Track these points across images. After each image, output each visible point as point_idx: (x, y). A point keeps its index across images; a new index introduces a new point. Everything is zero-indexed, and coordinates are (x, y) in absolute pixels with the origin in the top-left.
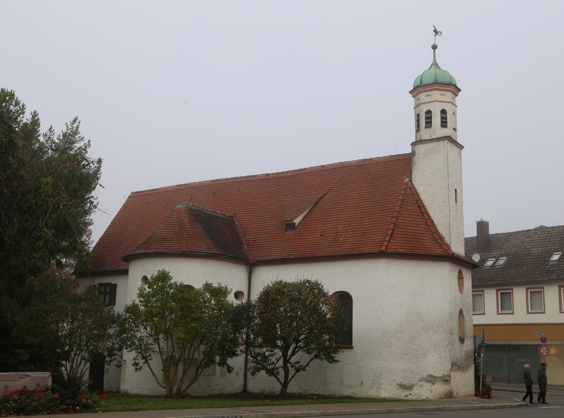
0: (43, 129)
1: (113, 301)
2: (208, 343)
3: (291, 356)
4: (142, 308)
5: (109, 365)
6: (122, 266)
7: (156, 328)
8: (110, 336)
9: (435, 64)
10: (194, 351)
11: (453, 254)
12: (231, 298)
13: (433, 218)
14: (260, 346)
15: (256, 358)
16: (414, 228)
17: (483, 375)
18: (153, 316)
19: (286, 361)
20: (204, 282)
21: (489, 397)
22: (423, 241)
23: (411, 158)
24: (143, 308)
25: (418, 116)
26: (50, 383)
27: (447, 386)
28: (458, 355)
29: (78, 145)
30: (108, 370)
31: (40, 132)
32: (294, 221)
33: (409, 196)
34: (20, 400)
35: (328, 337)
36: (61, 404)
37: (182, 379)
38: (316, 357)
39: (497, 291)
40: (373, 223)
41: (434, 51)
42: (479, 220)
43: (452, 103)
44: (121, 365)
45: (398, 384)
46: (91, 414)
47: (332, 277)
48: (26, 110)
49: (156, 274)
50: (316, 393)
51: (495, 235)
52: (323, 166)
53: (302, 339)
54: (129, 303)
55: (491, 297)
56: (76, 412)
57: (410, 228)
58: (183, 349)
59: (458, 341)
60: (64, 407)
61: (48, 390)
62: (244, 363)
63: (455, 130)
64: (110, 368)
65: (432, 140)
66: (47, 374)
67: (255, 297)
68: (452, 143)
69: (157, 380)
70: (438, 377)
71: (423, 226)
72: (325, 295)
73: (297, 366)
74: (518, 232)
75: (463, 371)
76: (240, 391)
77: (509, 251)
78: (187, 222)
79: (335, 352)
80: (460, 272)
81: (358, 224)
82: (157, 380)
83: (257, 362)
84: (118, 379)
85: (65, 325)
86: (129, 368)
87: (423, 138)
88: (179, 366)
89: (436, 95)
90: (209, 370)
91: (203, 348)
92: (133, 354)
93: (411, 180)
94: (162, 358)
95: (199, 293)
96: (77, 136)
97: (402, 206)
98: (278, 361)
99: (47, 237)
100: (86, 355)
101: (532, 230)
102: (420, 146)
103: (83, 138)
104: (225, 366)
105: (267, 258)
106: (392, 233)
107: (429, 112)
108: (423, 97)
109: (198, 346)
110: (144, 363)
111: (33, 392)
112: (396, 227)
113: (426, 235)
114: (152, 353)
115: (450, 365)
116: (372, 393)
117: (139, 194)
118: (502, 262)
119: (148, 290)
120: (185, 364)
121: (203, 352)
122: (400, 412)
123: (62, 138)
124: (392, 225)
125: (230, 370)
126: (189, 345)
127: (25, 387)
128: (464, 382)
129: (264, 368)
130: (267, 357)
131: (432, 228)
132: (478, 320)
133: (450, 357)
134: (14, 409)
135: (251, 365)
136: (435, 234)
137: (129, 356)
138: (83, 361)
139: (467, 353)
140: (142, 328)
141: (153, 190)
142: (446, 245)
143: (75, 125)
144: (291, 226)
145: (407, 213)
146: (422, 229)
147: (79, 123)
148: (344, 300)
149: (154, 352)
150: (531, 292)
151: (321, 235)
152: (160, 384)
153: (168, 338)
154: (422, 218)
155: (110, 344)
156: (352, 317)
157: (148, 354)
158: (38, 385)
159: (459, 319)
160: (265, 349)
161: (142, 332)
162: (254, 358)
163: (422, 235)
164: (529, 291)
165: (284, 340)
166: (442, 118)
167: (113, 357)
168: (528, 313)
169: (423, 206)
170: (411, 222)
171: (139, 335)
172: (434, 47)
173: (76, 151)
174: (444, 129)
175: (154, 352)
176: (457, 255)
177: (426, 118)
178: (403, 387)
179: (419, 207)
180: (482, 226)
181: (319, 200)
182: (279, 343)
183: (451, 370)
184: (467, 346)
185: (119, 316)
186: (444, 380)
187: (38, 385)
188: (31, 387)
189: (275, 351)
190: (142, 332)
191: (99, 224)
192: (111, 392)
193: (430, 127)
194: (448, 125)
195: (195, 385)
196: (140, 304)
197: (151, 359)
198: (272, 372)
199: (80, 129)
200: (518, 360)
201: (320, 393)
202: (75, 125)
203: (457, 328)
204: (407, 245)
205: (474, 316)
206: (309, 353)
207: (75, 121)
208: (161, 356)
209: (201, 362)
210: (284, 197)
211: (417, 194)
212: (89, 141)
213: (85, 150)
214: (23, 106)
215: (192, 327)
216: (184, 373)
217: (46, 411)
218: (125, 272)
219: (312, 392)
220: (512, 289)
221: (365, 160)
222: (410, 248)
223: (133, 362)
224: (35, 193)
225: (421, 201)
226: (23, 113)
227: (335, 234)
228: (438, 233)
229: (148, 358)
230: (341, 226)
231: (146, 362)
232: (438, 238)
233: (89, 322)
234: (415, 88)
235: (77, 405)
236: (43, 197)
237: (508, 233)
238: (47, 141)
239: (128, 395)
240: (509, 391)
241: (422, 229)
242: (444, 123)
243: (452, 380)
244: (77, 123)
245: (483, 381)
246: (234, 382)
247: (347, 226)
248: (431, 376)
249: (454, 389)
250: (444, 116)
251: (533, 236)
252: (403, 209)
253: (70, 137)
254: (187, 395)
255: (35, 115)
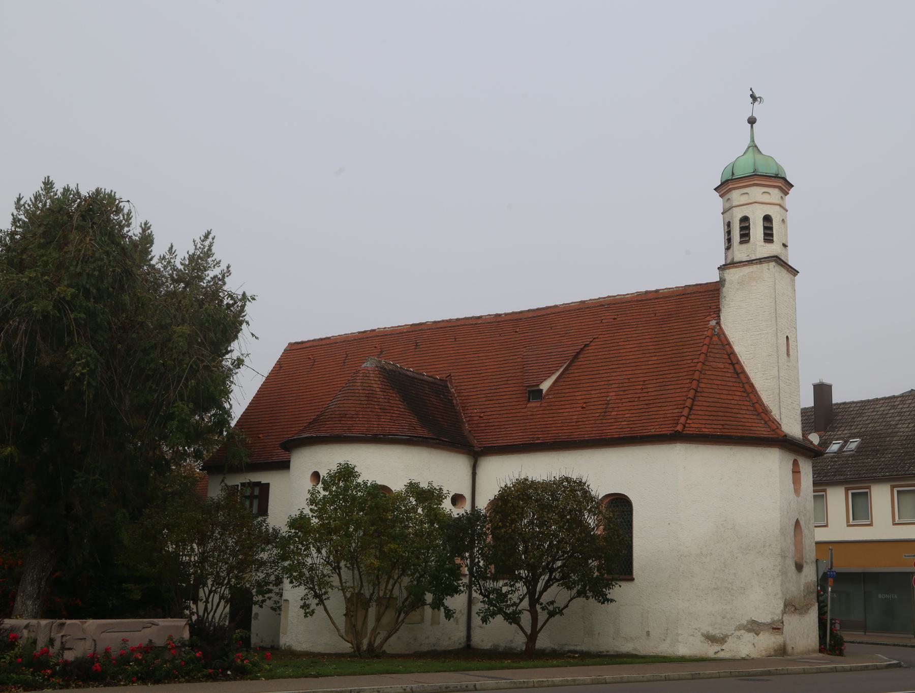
0: (158, 250)
1: (264, 510)
2: (413, 574)
3: (541, 593)
4: (315, 521)
5: (261, 607)
6: (281, 455)
7: (336, 552)
8: (262, 563)
9: (753, 146)
10: (393, 586)
11: (786, 436)
12: (447, 505)
13: (753, 381)
14: (495, 578)
15: (488, 597)
16: (725, 397)
17: (831, 620)
18: (330, 533)
19: (534, 601)
20: (406, 482)
21: (841, 654)
22: (739, 416)
23: (718, 290)
24: (317, 521)
25: (729, 224)
26: (186, 635)
27: (778, 637)
28: (794, 589)
29: (211, 274)
30: (257, 614)
31: (153, 254)
32: (541, 387)
33: (717, 347)
34: (146, 662)
35: (596, 563)
36: (205, 667)
37: (375, 629)
38: (580, 594)
39: (847, 490)
40: (662, 388)
41: (752, 127)
42: (817, 381)
43: (780, 205)
44: (280, 608)
45: (703, 635)
46: (249, 681)
47: (602, 472)
48: (133, 220)
49: (334, 468)
50: (578, 648)
51: (841, 404)
52: (583, 302)
53: (559, 567)
54: (295, 513)
55: (837, 498)
56: (227, 678)
57: (718, 396)
58: (376, 584)
59: (793, 568)
60: (210, 671)
61: (184, 645)
62: (466, 604)
63: (785, 246)
64: (260, 614)
65: (750, 262)
66: (182, 622)
67: (482, 504)
68: (782, 266)
69: (338, 630)
70: (764, 624)
71: (739, 394)
72: (592, 499)
73: (551, 608)
74: (877, 399)
75: (800, 614)
76: (460, 646)
77: (863, 430)
78: (378, 390)
79: (609, 586)
80: (795, 463)
81: (639, 391)
82: (338, 630)
83: (490, 603)
84: (276, 629)
85: (195, 546)
86: (293, 613)
87: (736, 260)
88: (370, 610)
89: (756, 193)
90: (414, 615)
91: (406, 580)
92: (302, 591)
93: (718, 323)
94: (345, 597)
95: (399, 497)
96: (210, 260)
97: (707, 363)
98: (521, 600)
99: (183, 416)
100: (227, 592)
101: (898, 397)
102: (732, 271)
103: (219, 263)
104: (442, 609)
105: (501, 443)
106: (692, 405)
107: (745, 219)
108: (737, 196)
109: (399, 577)
110: (317, 605)
111: (164, 648)
112: (699, 394)
113: (743, 407)
114: (330, 590)
115: (782, 605)
116: (664, 649)
117: (300, 346)
118: (853, 444)
119: (323, 493)
120: (379, 604)
121: (406, 588)
122: (711, 678)
123: (187, 263)
124: (692, 392)
125: (449, 614)
126: (385, 577)
127: (150, 641)
128: (804, 631)
129: (500, 611)
130: (506, 595)
131: (752, 395)
132: (822, 535)
133: (783, 593)
134: (137, 674)
135: (479, 606)
136: (757, 405)
137: (293, 594)
138: (222, 603)
139: (807, 586)
140: (313, 551)
141: (321, 339)
142: (774, 421)
143: (207, 243)
144: (537, 394)
145: (714, 373)
146: (737, 398)
147: (213, 239)
148: (620, 507)
149: (332, 587)
150: (898, 492)
151: (583, 408)
152: (342, 637)
153: (353, 568)
154: (738, 380)
155: (262, 575)
156: (631, 533)
157: (323, 591)
158: (170, 637)
159: (795, 535)
160: (501, 583)
161: (315, 557)
162: (485, 596)
163: (737, 407)
164: (895, 490)
165: (532, 568)
166: (765, 228)
167: (267, 596)
168: (895, 524)
169: (738, 362)
170: (720, 387)
171: (309, 561)
172: (752, 121)
173: (209, 282)
174: (768, 245)
175: (332, 587)
176: (791, 437)
177: (742, 229)
178: (711, 639)
179: (733, 364)
180: (822, 391)
181: (578, 353)
182: (524, 573)
183: (784, 612)
184: (806, 576)
185: (276, 531)
186: (774, 629)
187: (170, 637)
188: (160, 642)
189: (517, 585)
190: (315, 557)
191: (241, 395)
192: (262, 648)
193: (748, 241)
194: (775, 238)
195: (394, 638)
196: (311, 514)
197: (328, 598)
198: (513, 618)
199: (214, 249)
200: (880, 596)
201: (584, 648)
202: (207, 243)
203: (792, 548)
204: (715, 422)
205: (816, 529)
206: (570, 588)
207: (206, 237)
208: (344, 593)
209: (403, 603)
210: (524, 350)
211: (729, 344)
212: (228, 267)
213: (223, 280)
214: (129, 214)
215: (391, 550)
216: (378, 619)
217: (183, 677)
218: (285, 466)
219: (572, 648)
220: (869, 488)
221: (647, 292)
222: (720, 427)
223: (302, 603)
224: (162, 349)
225: (735, 355)
226: (128, 226)
227: (604, 406)
228: (762, 404)
229: (324, 597)
230: (614, 394)
231: (321, 602)
232: (761, 411)
233: (231, 542)
234: (724, 183)
235: (229, 669)
236: (175, 356)
237: (862, 402)
238: (165, 267)
239: (291, 654)
240: (867, 643)
241: (737, 398)
242: (768, 236)
243: (786, 628)
244: (210, 240)
245: (831, 629)
246: (451, 633)
247: (622, 393)
248: (754, 622)
249: (788, 642)
250: (768, 225)
251: (900, 406)
252: (707, 368)
253: (199, 261)
254: (384, 652)
255: (146, 227)
